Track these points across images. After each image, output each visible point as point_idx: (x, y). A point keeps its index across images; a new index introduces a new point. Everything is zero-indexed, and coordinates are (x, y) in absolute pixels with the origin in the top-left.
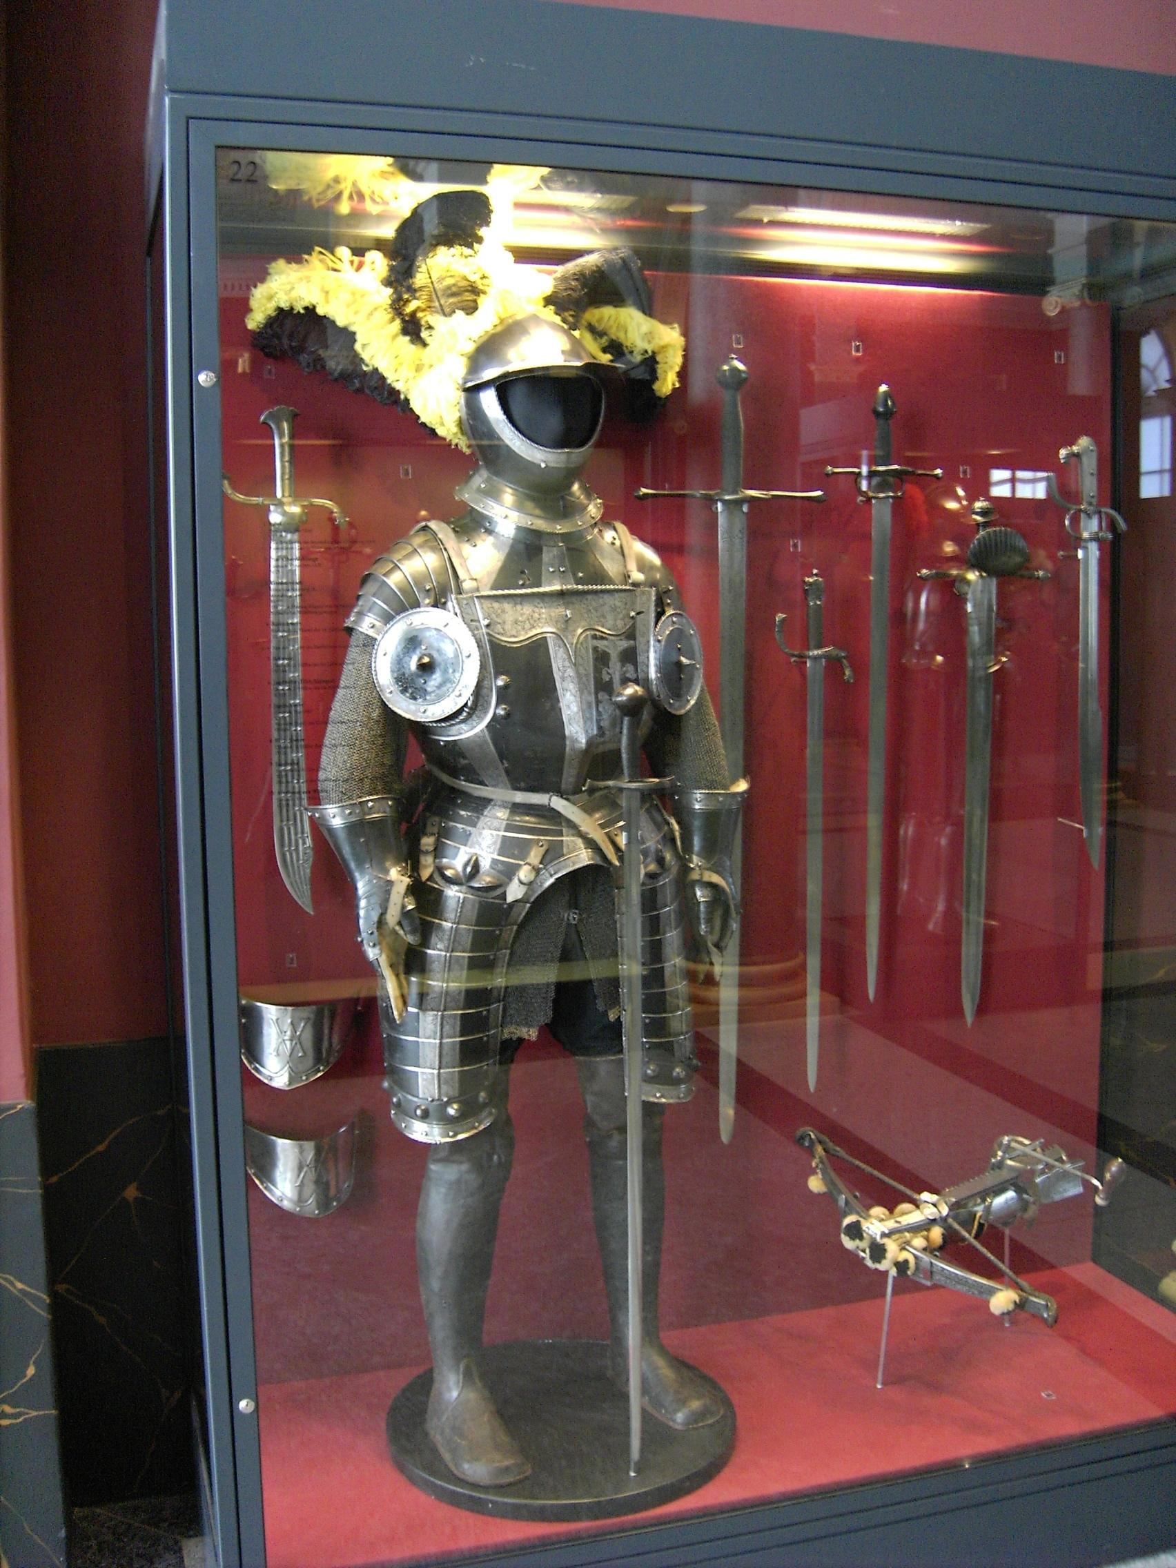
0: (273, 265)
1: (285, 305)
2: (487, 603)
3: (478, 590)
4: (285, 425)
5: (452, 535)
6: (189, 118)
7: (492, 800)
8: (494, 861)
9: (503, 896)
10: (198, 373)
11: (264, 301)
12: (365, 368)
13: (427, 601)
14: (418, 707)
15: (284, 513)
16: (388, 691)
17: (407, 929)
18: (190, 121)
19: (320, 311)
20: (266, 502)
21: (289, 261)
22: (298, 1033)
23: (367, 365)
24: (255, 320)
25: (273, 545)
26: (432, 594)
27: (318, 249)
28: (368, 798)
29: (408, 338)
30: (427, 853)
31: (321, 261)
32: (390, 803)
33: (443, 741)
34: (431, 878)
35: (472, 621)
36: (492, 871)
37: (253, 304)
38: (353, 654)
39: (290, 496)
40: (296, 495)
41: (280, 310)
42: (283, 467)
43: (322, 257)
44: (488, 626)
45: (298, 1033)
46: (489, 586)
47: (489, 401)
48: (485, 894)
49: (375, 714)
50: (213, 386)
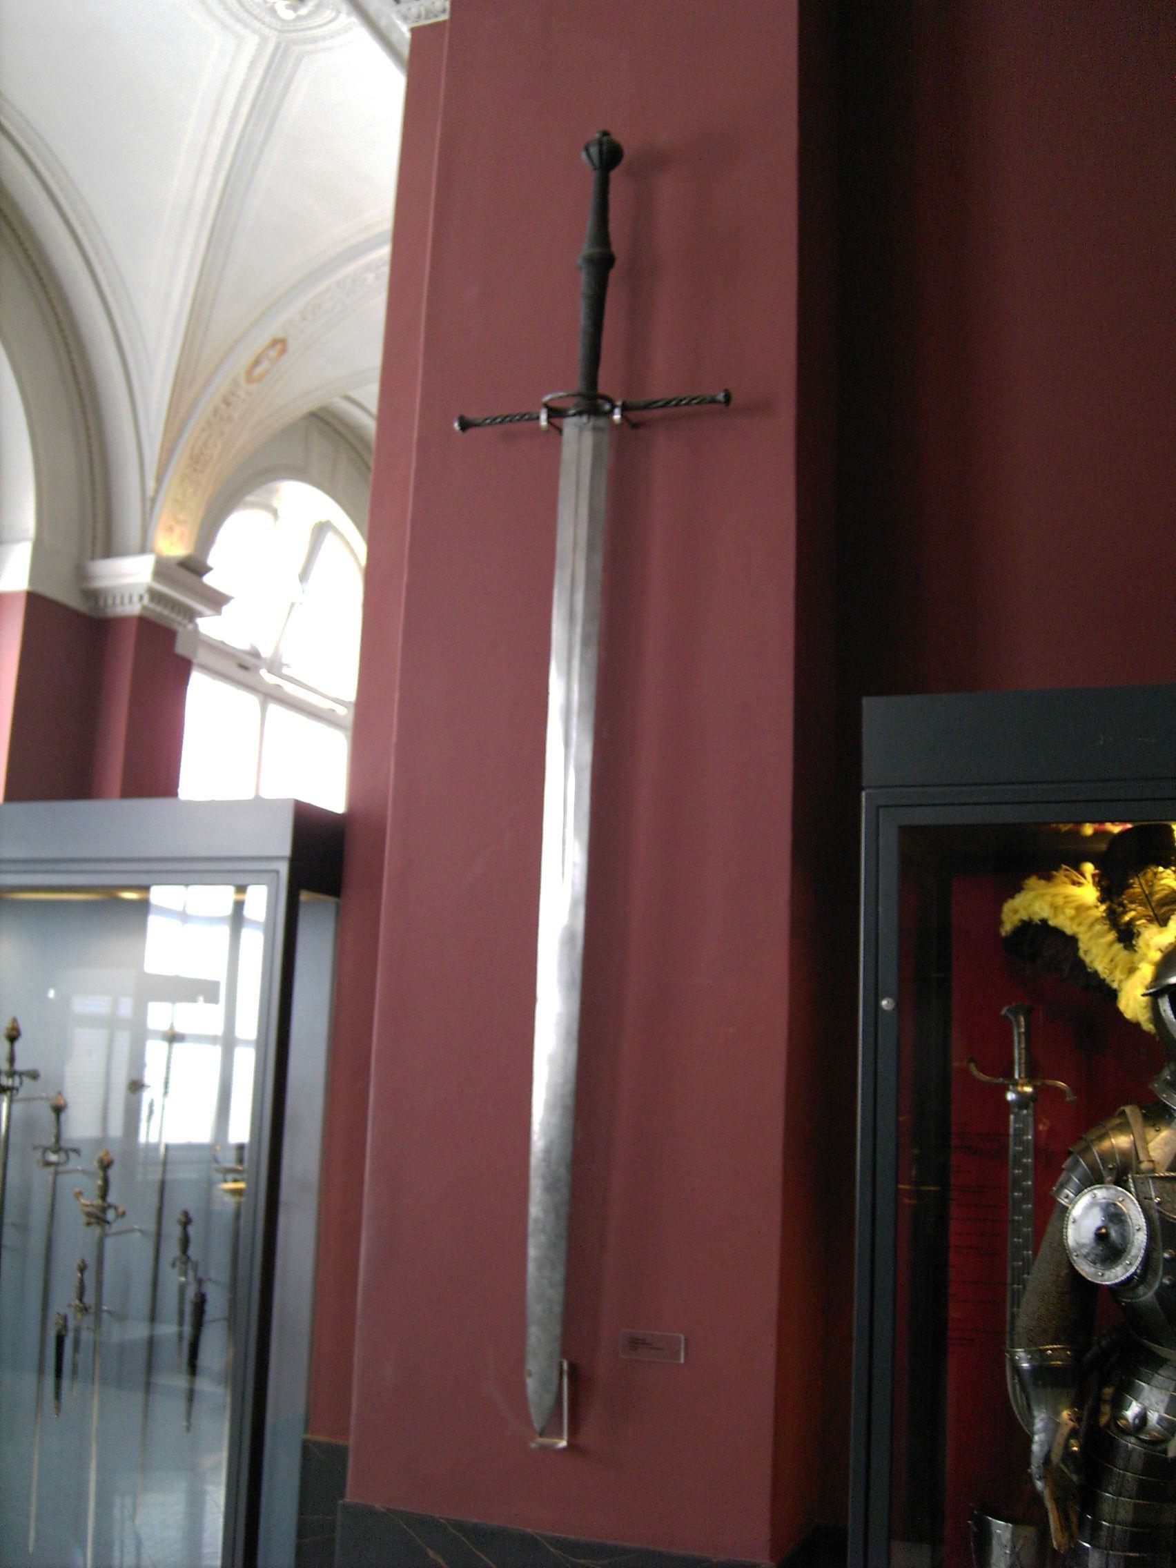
0: (1027, 881)
1: (1025, 918)
2: (1159, 1183)
3: (1153, 1170)
4: (1022, 1019)
5: (1140, 1120)
6: (879, 807)
7: (1169, 1360)
8: (1161, 1419)
9: (1165, 1451)
10: (881, 1000)
11: (1011, 914)
12: (1089, 970)
13: (1109, 1179)
14: (1096, 1270)
15: (1018, 1093)
16: (1075, 1254)
17: (1072, 1468)
18: (880, 810)
19: (1051, 923)
20: (1005, 1082)
21: (1041, 877)
22: (1017, 1549)
23: (1090, 968)
24: (1007, 927)
25: (1012, 1117)
26: (1115, 1172)
27: (1064, 866)
28: (1047, 1347)
29: (1121, 945)
30: (1105, 1401)
31: (1066, 876)
32: (1069, 1353)
33: (1124, 1302)
34: (1108, 1426)
35: (1146, 1198)
36: (1158, 1426)
37: (1004, 917)
38: (1055, 1215)
39: (1026, 1077)
40: (1031, 1077)
41: (1023, 922)
42: (1020, 1053)
43: (1067, 872)
44: (1159, 1204)
45: (1017, 1549)
46: (1166, 1167)
47: (1165, 1005)
48: (1151, 1447)
49: (1064, 1272)
50: (894, 1009)
